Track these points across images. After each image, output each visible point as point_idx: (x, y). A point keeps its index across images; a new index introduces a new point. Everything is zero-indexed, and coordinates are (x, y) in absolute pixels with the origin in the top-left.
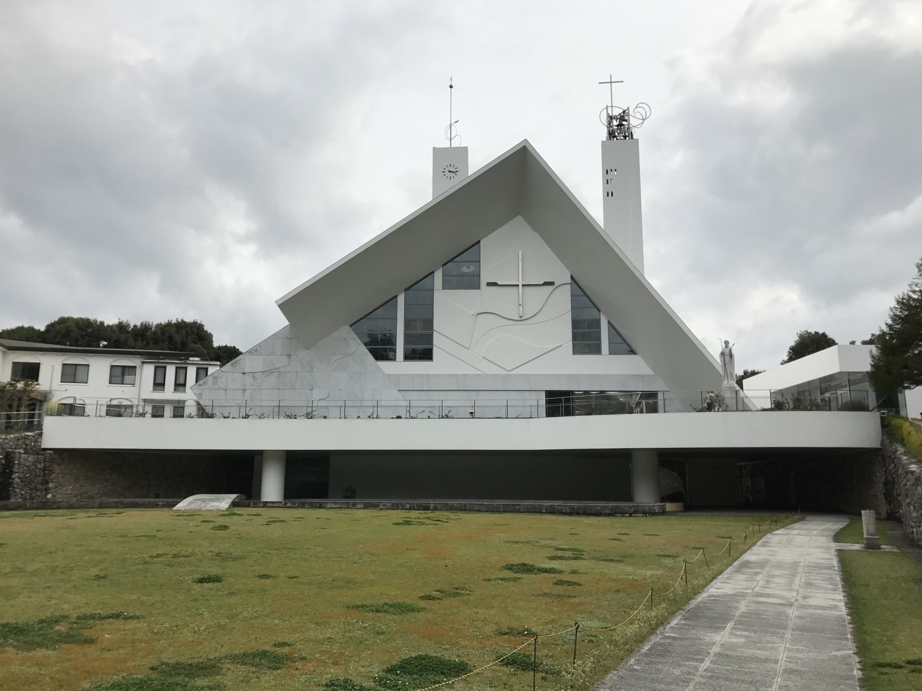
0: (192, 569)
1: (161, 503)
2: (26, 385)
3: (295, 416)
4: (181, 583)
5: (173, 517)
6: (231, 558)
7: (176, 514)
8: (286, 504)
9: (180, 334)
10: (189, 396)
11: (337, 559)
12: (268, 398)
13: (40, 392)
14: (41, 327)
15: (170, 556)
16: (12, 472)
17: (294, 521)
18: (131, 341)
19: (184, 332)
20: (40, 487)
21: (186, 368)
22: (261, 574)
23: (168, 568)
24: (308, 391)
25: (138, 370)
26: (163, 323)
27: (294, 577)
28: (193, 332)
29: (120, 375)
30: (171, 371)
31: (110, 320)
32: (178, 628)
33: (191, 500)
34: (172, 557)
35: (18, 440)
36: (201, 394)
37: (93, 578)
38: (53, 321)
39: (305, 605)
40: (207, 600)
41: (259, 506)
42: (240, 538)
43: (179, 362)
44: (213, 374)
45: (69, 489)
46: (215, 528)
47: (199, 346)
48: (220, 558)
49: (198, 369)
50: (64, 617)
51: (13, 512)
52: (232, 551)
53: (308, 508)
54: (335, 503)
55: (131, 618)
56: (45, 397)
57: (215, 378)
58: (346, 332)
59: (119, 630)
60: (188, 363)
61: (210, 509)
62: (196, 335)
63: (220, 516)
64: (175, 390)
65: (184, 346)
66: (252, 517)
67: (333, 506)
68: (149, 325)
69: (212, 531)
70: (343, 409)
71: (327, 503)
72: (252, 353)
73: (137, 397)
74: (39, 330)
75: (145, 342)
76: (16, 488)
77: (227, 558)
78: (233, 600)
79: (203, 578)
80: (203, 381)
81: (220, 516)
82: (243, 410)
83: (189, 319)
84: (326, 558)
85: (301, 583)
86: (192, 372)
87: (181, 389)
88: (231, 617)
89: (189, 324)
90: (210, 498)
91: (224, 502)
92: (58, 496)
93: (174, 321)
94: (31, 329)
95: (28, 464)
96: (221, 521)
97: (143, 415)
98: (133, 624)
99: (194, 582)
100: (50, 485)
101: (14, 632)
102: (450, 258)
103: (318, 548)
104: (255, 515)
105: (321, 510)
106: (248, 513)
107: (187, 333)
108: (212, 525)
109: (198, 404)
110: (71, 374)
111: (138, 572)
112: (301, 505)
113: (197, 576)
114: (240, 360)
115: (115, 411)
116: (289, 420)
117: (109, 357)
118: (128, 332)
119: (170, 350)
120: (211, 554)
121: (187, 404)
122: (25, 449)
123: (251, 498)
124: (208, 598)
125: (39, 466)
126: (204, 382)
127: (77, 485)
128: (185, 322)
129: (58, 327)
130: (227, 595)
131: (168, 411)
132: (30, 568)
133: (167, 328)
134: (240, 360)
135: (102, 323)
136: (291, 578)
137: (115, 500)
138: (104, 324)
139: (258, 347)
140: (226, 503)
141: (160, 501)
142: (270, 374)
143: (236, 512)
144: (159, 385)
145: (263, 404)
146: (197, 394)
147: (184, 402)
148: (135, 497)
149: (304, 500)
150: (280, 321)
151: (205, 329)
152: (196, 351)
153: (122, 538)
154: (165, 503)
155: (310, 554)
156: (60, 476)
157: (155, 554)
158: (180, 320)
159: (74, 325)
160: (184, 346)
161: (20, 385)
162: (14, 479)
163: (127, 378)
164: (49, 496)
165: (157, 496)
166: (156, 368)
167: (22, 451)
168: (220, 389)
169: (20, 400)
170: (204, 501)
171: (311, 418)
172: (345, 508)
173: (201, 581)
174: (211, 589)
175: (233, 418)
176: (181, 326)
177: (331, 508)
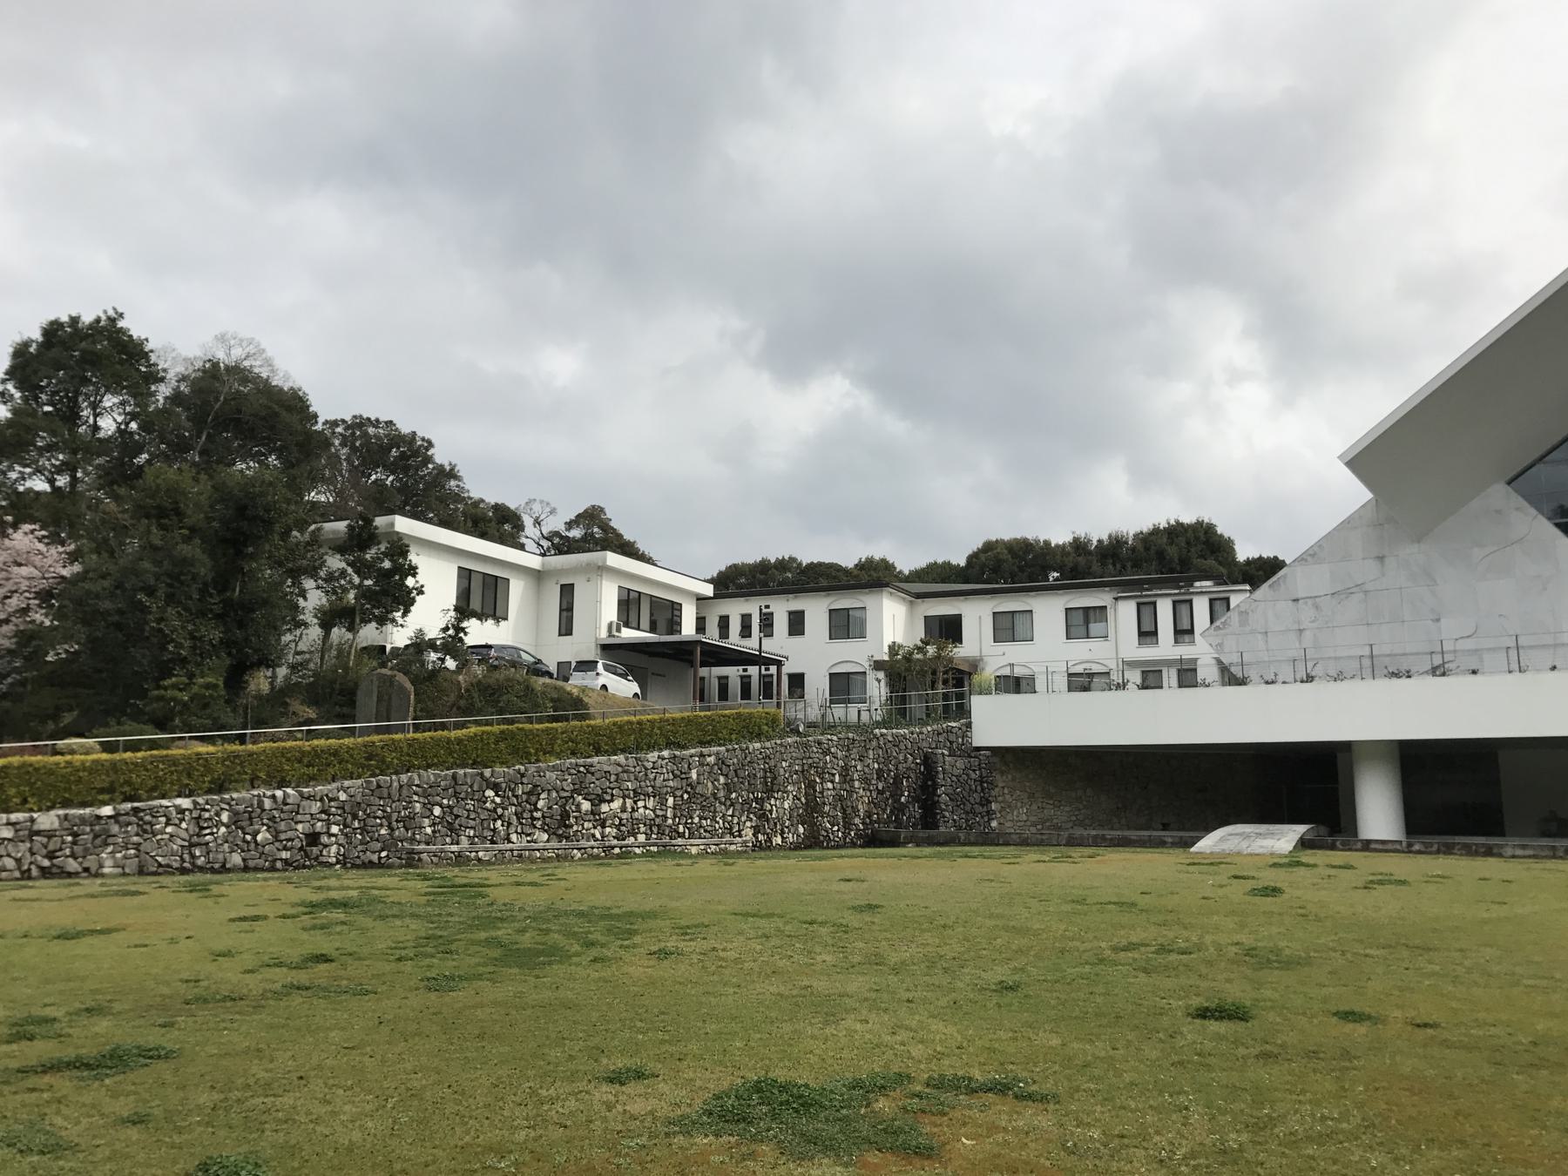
0: (1191, 982)
1: (1170, 840)
2: (127, 424)
3: (1408, 672)
4: (1161, 1014)
5: (1180, 867)
6: (1279, 962)
7: (1188, 861)
8: (1410, 845)
9: (1177, 545)
10: (1201, 650)
11: (1538, 982)
12: (1349, 642)
13: (965, 660)
14: (960, 560)
15: (1153, 949)
16: (935, 786)
17: (1426, 882)
18: (1096, 567)
19: (1182, 541)
20: (978, 809)
21: (1190, 602)
22: (1341, 1009)
23: (1142, 975)
24: (1430, 622)
25: (1110, 612)
26: (1145, 530)
27: (1426, 1025)
28: (1197, 538)
29: (1082, 623)
30: (1165, 609)
31: (1059, 536)
32: (1126, 1141)
33: (1222, 834)
34: (1156, 952)
35: (939, 734)
36: (1220, 645)
37: (994, 987)
38: (975, 550)
39: (1458, 1113)
40: (1209, 1067)
41: (1354, 847)
42: (1303, 916)
43: (1176, 591)
44: (1238, 605)
45: (1021, 813)
46: (1255, 892)
47: (1211, 562)
48: (1253, 961)
49: (1211, 601)
50: (902, 1078)
51: (938, 849)
52: (1282, 944)
53: (1461, 855)
54: (1524, 847)
55: (1030, 1097)
56: (975, 665)
57: (1244, 614)
58: (1500, 495)
59: (993, 1128)
60: (1193, 593)
61: (1257, 852)
62: (1204, 543)
63: (1271, 866)
64: (1176, 641)
65: (1185, 564)
66: (1333, 872)
67: (1519, 852)
68: (1123, 536)
69: (1249, 898)
70: (1513, 653)
71: (1502, 846)
72: (1306, 560)
73: (1114, 656)
74: (959, 565)
75: (1118, 566)
76: (944, 810)
77: (1269, 961)
78: (1263, 1075)
79: (1207, 1009)
80: (1223, 620)
81: (1271, 866)
82: (1301, 667)
83: (1188, 518)
84: (1508, 977)
85: (1446, 1044)
86: (1201, 607)
87: (1187, 638)
88: (1259, 1127)
89: (1189, 526)
90: (1257, 831)
91: (1283, 838)
92: (1008, 824)
93: (1163, 525)
94: (947, 565)
95: (956, 772)
96: (1270, 878)
97: (1122, 686)
98: (1030, 1116)
99: (1189, 1014)
100: (994, 806)
101: (795, 1106)
102: (1537, 455)
103: (1488, 949)
104: (1340, 867)
105: (1491, 860)
106: (1328, 862)
107: (1188, 543)
108: (1250, 884)
109: (1219, 662)
110: (1007, 628)
111: (1081, 981)
112: (1443, 849)
113: (1196, 1002)
114: (1285, 576)
115: (1081, 682)
116: (1395, 681)
117: (1061, 595)
118: (1090, 553)
119: (1162, 573)
120: (1234, 949)
121: (1199, 662)
122: (950, 749)
123: (1340, 832)
124: (1212, 1060)
125: (973, 776)
126: (1224, 623)
127: (1034, 807)
128: (1182, 524)
129: (983, 557)
130: (1257, 1056)
131: (1169, 677)
132: (894, 958)
133: (1153, 538)
134: (1285, 576)
135: (1047, 543)
136: (1418, 1026)
137: (1094, 833)
138: (1050, 544)
139: (1316, 549)
140: (1287, 841)
141: (1168, 836)
142: (1347, 598)
143: (1304, 860)
144: (1148, 634)
145: (1339, 654)
146: (1214, 645)
147: (1196, 660)
148: (1129, 829)
149: (1449, 839)
150: (1356, 494)
151: (1219, 532)
152: (1206, 571)
153: (1074, 905)
154: (1177, 840)
155: (1466, 963)
156: (1006, 791)
157: (1124, 942)
158: (1172, 522)
159: (1006, 551)
160: (1185, 564)
161: (931, 650)
162: (939, 796)
163: (1095, 628)
164: (994, 824)
165: (1165, 827)
166: (1139, 605)
167: (946, 752)
168: (1253, 632)
169: (934, 673)
170: (1246, 836)
171: (1443, 674)
172: (1546, 857)
173: (1203, 1014)
174: (1219, 1038)
175: (1284, 683)
176: (1176, 531)
177: (1513, 857)
